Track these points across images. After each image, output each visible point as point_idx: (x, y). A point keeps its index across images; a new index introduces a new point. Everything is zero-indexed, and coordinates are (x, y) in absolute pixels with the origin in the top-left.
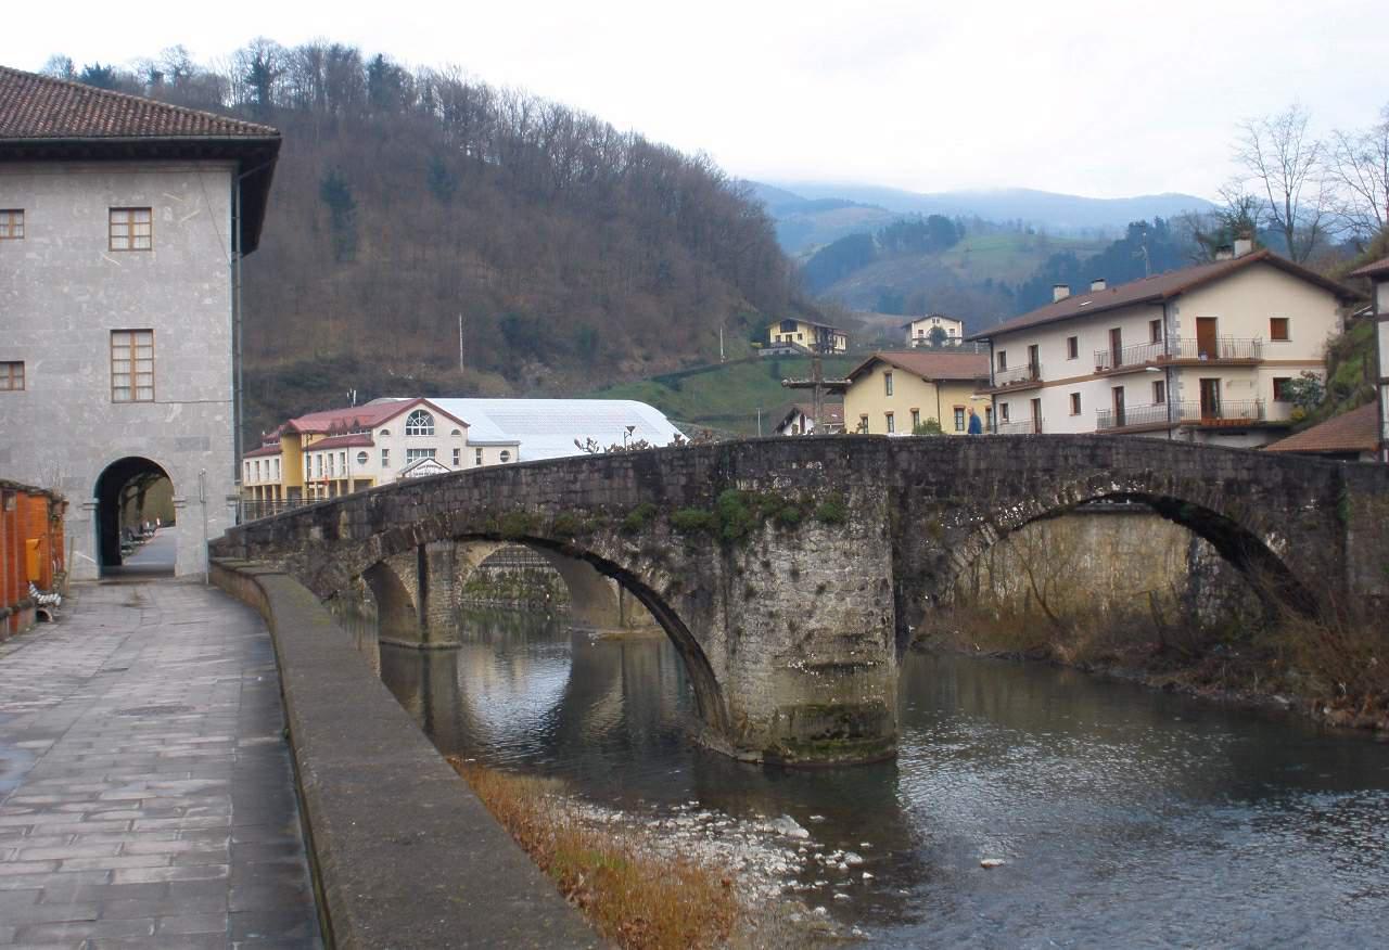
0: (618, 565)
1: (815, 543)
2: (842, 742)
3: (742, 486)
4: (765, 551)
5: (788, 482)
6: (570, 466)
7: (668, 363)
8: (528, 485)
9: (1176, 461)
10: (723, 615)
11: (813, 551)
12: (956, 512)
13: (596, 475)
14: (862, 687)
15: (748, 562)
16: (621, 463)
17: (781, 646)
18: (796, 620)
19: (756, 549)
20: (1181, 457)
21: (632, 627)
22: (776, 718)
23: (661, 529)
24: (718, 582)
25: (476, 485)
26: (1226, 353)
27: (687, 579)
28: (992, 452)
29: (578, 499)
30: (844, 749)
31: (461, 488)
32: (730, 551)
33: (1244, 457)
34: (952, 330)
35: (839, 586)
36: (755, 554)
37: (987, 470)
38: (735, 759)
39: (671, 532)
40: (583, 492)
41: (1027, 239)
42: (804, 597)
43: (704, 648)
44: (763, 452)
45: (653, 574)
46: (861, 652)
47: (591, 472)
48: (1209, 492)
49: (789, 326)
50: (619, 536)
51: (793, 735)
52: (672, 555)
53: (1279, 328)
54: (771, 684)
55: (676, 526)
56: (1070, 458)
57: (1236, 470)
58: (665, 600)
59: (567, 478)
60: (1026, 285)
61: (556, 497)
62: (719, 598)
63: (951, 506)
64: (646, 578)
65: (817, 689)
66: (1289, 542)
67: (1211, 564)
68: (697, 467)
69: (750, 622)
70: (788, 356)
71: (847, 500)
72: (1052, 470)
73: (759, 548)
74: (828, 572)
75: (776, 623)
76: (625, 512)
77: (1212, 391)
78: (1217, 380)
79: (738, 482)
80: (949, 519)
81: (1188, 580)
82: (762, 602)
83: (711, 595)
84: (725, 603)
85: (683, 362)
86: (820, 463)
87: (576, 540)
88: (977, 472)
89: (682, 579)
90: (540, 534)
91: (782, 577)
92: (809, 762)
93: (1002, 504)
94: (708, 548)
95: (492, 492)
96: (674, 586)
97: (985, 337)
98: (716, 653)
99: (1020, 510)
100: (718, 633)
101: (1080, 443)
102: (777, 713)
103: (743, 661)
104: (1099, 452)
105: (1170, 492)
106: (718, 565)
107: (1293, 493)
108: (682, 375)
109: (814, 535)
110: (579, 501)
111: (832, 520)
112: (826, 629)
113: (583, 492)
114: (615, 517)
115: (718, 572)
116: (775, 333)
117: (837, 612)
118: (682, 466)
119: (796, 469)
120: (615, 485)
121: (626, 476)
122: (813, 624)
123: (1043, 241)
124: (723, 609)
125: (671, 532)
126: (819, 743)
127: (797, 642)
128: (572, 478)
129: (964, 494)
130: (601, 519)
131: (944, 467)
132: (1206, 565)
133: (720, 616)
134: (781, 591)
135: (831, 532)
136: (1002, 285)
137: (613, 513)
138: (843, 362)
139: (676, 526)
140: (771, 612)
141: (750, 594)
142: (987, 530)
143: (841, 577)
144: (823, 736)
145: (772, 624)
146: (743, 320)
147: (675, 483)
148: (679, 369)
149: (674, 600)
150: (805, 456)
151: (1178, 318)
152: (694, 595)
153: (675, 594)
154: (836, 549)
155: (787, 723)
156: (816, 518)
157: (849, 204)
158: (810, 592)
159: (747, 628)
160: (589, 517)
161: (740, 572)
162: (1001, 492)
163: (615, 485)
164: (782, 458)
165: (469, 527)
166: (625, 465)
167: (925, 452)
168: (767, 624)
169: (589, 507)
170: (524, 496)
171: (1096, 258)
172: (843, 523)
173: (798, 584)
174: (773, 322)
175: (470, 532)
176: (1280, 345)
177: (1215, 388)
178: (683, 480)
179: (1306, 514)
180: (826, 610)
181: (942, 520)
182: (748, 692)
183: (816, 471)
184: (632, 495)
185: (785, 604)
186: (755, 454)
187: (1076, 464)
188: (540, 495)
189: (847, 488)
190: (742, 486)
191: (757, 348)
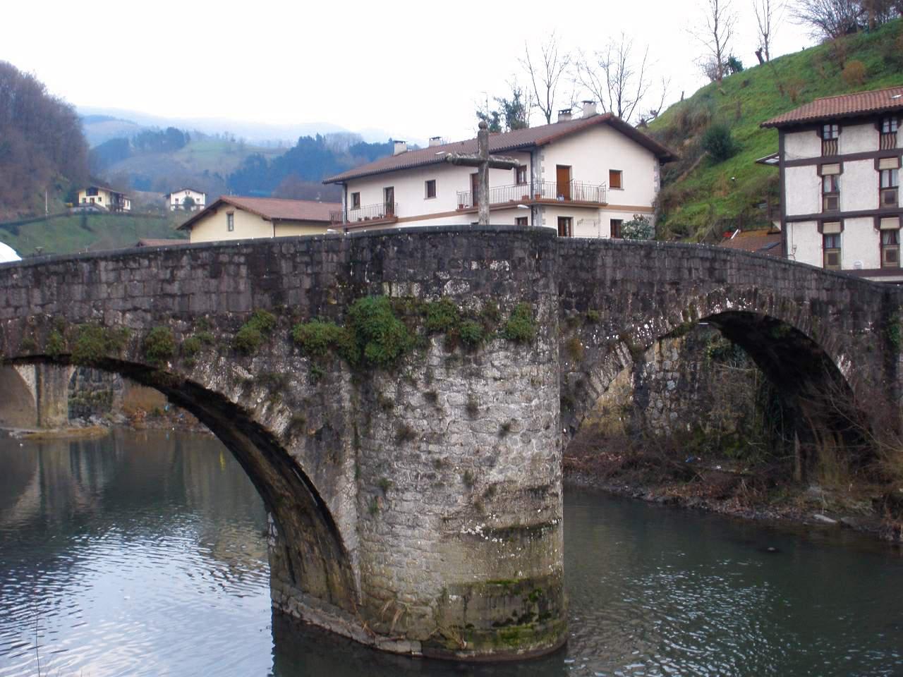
0: (226, 398)
1: (498, 368)
2: (532, 627)
3: (396, 291)
4: (429, 378)
5: (465, 287)
6: (166, 259)
7: (9, 215)
8: (109, 284)
9: (776, 278)
10: (353, 461)
11: (495, 379)
12: (594, 329)
13: (200, 272)
14: (548, 553)
15: (400, 394)
16: (232, 256)
17: (451, 505)
18: (473, 470)
19: (415, 376)
20: (780, 275)
21: (50, 427)
22: (443, 599)
23: (280, 348)
24: (347, 418)
25: (38, 283)
26: (577, 196)
27: (311, 415)
28: (627, 260)
29: (175, 305)
30: (537, 636)
31: (14, 287)
32: (368, 377)
33: (823, 277)
34: (198, 200)
35: (524, 424)
36: (414, 383)
37: (624, 281)
38: (372, 648)
39: (291, 352)
40: (183, 295)
41: (231, 147)
42: (484, 442)
43: (331, 506)
44: (428, 246)
45: (270, 409)
46: (546, 508)
47: (193, 268)
48: (799, 312)
49: (92, 191)
50: (227, 358)
51: (468, 622)
52: (293, 383)
53: (615, 178)
54: (436, 555)
55: (300, 344)
56: (693, 271)
57: (818, 289)
58: (282, 445)
59: (162, 277)
60: (232, 175)
61: (146, 303)
62: (348, 440)
63: (590, 321)
64: (260, 416)
65: (500, 561)
66: (853, 366)
67: (665, 379)
68: (325, 265)
69: (404, 474)
70: (91, 213)
71: (535, 312)
72: (678, 284)
73: (419, 375)
74: (512, 406)
75: (444, 476)
76: (235, 324)
77: (565, 226)
78: (570, 219)
79: (386, 287)
80: (587, 337)
81: (634, 393)
82: (424, 446)
83: (338, 435)
84: (356, 446)
85: (19, 213)
86: (507, 264)
87: (172, 363)
88: (614, 282)
89: (305, 416)
90: (125, 355)
91: (453, 414)
92: (493, 655)
93: (636, 320)
94: (336, 374)
95: (59, 294)
96: (296, 425)
97: (340, 181)
98: (345, 511)
99: (650, 328)
100: (347, 486)
101: (701, 255)
102: (444, 592)
103: (392, 525)
104: (717, 265)
105: (771, 311)
106: (347, 396)
107: (856, 313)
108: (19, 224)
109: (498, 357)
110: (177, 308)
111: (518, 339)
112: (511, 481)
113: (183, 295)
114: (224, 331)
115: (347, 405)
116: (83, 197)
117: (523, 459)
118: (307, 264)
119: (477, 270)
120: (223, 288)
121: (237, 275)
122: (494, 476)
123: (242, 147)
124: (352, 453)
125: (291, 352)
126: (504, 631)
127: (474, 500)
128: (168, 276)
129: (601, 308)
130: (206, 334)
131: (583, 275)
132: (657, 381)
133: (349, 463)
134: (453, 433)
135: (518, 353)
136: (216, 175)
137: (220, 325)
138: (131, 218)
139: (300, 344)
140: (438, 461)
141: (405, 435)
142: (622, 351)
143: (528, 412)
144: (509, 621)
145: (439, 477)
146: (59, 187)
147: (298, 285)
148: (17, 219)
149: (294, 443)
150: (488, 253)
151: (543, 164)
152: (319, 435)
153: (296, 436)
154: (522, 376)
155: (460, 606)
156: (502, 336)
157: (113, 119)
158: (491, 434)
159: (400, 481)
160: (189, 330)
161: (388, 406)
162: (635, 309)
163: (223, 288)
164: (458, 253)
165: (27, 347)
166: (236, 259)
167: (565, 257)
168: (431, 477)
169: (189, 317)
170: (104, 301)
171: (280, 158)
172: (530, 343)
173: (474, 424)
174: (81, 188)
175: (28, 353)
176: (615, 192)
177: (567, 225)
178: (307, 283)
179: (865, 336)
180: (512, 456)
181: (581, 339)
182: (399, 564)
183: (502, 272)
184: (244, 302)
185: (457, 449)
186: (416, 249)
187: (699, 278)
188: (124, 299)
189: (535, 297)
190: (396, 291)
191: (69, 207)
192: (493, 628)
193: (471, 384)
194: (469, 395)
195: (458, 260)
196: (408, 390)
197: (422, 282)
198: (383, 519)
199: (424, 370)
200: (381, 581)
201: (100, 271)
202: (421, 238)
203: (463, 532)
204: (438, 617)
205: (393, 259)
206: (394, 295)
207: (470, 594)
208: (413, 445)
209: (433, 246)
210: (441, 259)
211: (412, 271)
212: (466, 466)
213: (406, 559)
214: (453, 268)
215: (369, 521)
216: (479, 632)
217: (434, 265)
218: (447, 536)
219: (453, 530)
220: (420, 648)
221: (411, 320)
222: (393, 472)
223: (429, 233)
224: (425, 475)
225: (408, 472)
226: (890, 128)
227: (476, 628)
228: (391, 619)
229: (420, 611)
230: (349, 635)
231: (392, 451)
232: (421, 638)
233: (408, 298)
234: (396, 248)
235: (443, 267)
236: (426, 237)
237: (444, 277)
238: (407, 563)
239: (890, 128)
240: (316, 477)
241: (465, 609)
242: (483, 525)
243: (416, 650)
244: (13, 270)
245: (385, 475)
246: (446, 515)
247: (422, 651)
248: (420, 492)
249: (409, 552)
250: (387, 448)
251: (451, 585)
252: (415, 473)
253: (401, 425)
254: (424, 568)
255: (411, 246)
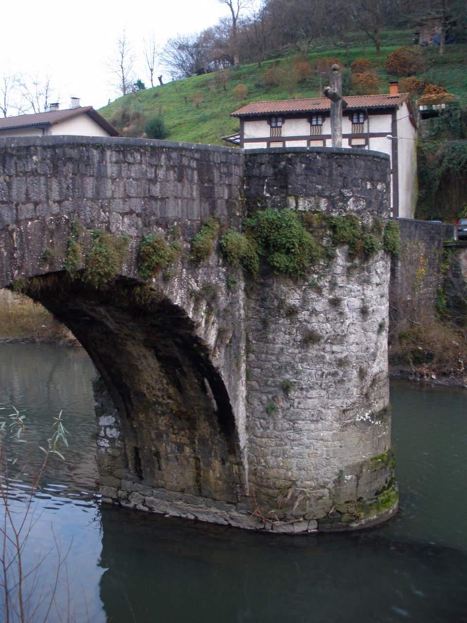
3: (304, 205)
4: (333, 285)
5: (363, 203)
15: (305, 301)
18: (365, 365)
19: (321, 283)
22: (339, 481)
31: (34, 173)
36: (319, 291)
44: (335, 165)
51: (360, 496)
69: (309, 373)
73: (324, 283)
75: (345, 372)
79: (292, 201)
82: (328, 347)
91: (352, 316)
92: (377, 519)
102: (341, 474)
127: (365, 391)
140: (340, 360)
141: (310, 338)
145: (341, 373)
155: (354, 484)
161: (292, 312)
164: (358, 174)
168: (335, 374)
186: (324, 168)
190: (304, 205)
192: (375, 497)
193: (363, 290)
194: (362, 299)
195: (358, 179)
196: (313, 296)
197: (329, 198)
198: (284, 417)
199: (329, 278)
200: (278, 473)
201: (106, 162)
202: (329, 158)
203: (357, 420)
204: (335, 495)
205: (301, 175)
206: (300, 208)
207: (361, 472)
208: (318, 347)
209: (339, 166)
210: (345, 177)
211: (320, 187)
212: (360, 362)
213: (307, 451)
214: (355, 186)
215: (264, 419)
216: (368, 502)
217: (340, 183)
218: (346, 425)
219: (351, 419)
220: (316, 526)
221: (318, 232)
222: (297, 373)
223: (337, 154)
224: (329, 374)
225: (313, 371)
226: (317, 122)
227: (365, 499)
228: (293, 505)
229: (318, 494)
230: (226, 523)
231: (296, 354)
232: (319, 517)
233: (316, 212)
234: (304, 165)
235: (347, 185)
236: (333, 157)
237: (348, 195)
238: (308, 454)
239: (317, 122)
240: (230, 384)
241: (358, 485)
242: (370, 411)
243: (312, 528)
244: (32, 148)
245: (288, 376)
246: (345, 407)
247: (317, 529)
248: (324, 389)
249: (311, 443)
250: (290, 351)
251: (348, 467)
252: (320, 373)
253: (306, 330)
254: (325, 456)
255: (320, 164)
